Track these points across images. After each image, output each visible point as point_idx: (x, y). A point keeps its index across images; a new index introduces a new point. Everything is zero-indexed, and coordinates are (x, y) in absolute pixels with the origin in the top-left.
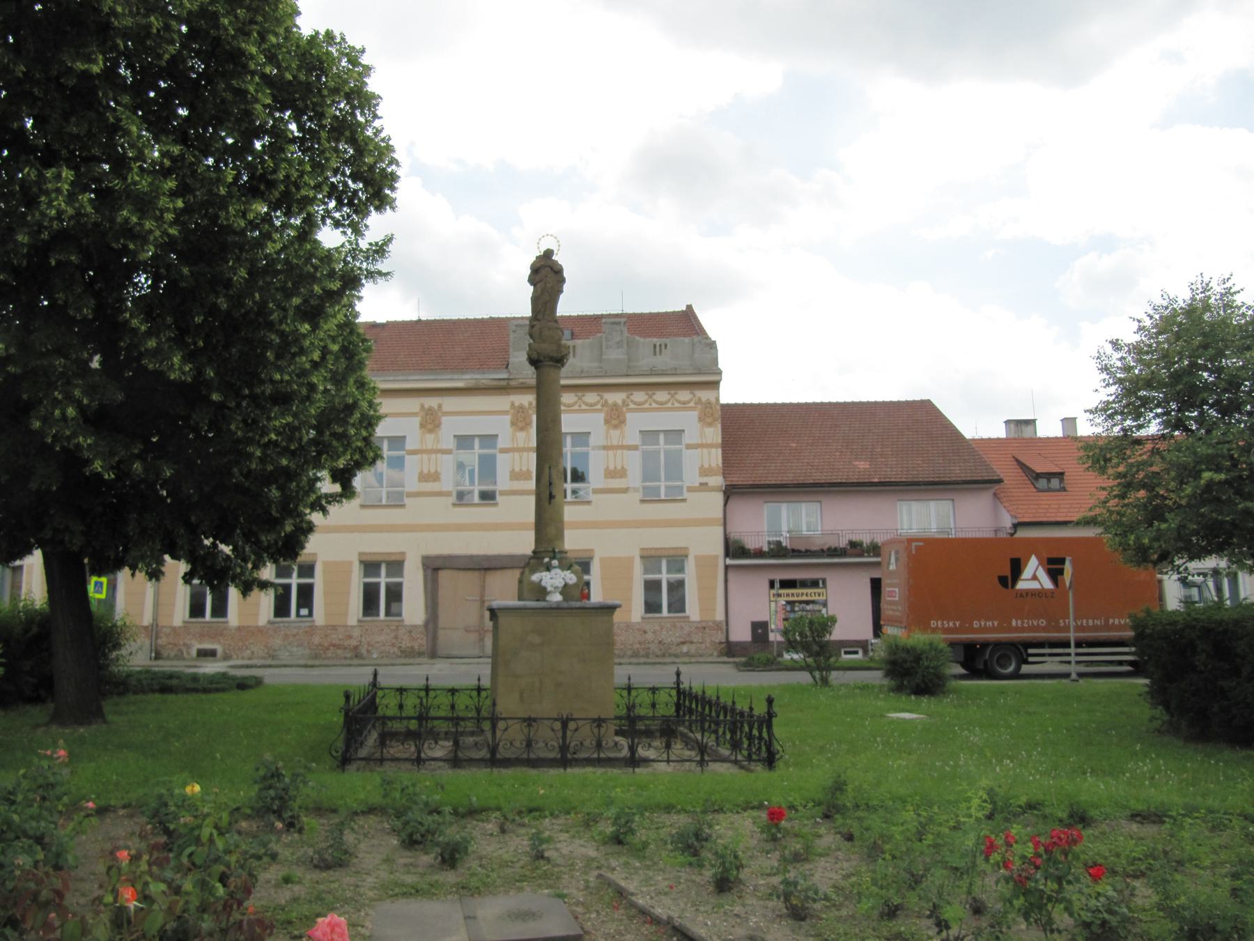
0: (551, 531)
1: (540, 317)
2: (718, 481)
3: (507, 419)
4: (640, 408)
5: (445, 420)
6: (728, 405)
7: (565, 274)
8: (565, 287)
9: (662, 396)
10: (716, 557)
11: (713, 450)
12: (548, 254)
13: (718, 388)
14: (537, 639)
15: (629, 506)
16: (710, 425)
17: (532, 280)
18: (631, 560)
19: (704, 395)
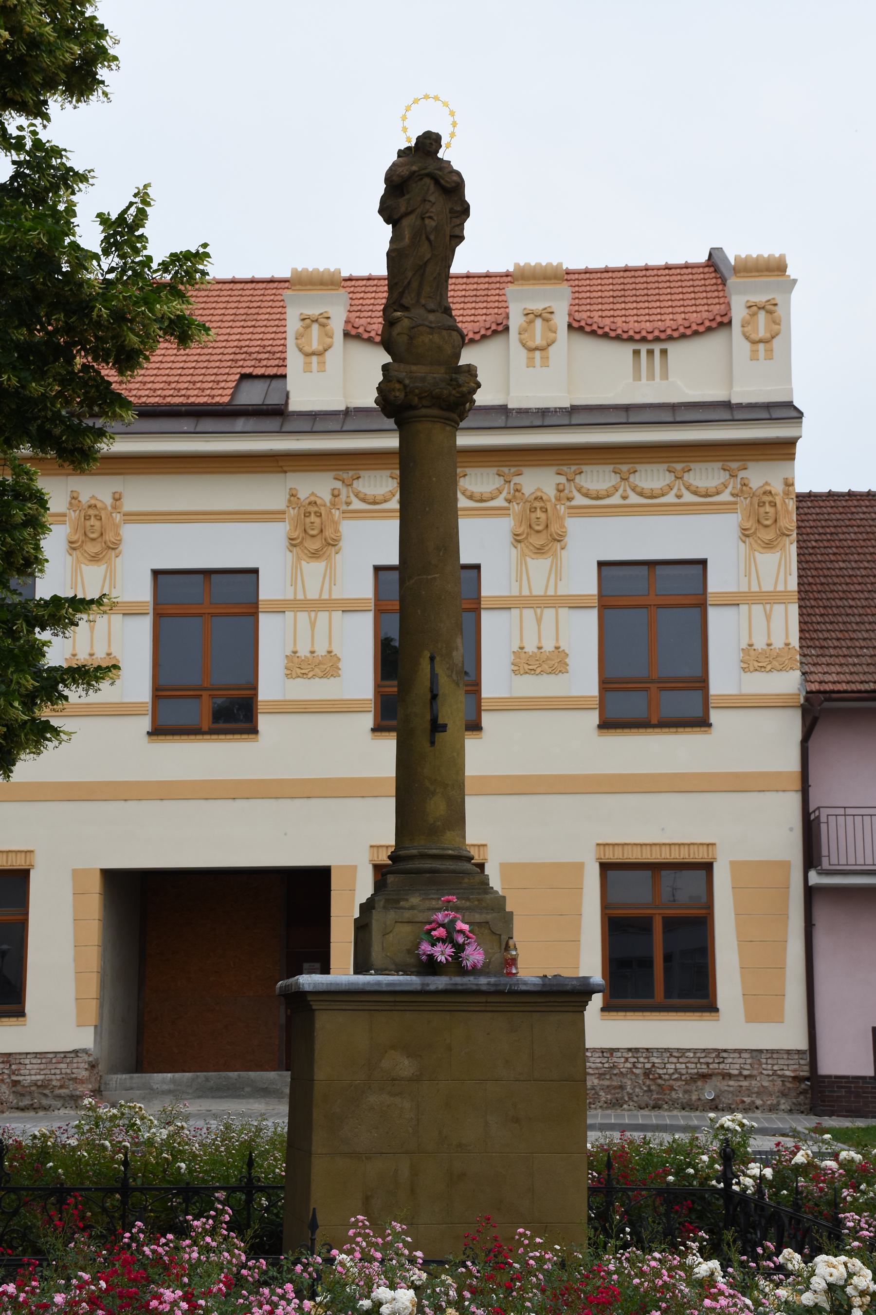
0: (437, 807)
1: (407, 300)
2: (789, 682)
3: (279, 531)
4: (598, 506)
5: (130, 533)
6: (810, 496)
7: (470, 195)
8: (469, 227)
9: (652, 477)
10: (785, 865)
11: (778, 610)
12: (428, 143)
13: (791, 457)
14: (405, 1066)
15: (577, 742)
16: (769, 546)
17: (387, 211)
18: (579, 867)
19: (760, 476)
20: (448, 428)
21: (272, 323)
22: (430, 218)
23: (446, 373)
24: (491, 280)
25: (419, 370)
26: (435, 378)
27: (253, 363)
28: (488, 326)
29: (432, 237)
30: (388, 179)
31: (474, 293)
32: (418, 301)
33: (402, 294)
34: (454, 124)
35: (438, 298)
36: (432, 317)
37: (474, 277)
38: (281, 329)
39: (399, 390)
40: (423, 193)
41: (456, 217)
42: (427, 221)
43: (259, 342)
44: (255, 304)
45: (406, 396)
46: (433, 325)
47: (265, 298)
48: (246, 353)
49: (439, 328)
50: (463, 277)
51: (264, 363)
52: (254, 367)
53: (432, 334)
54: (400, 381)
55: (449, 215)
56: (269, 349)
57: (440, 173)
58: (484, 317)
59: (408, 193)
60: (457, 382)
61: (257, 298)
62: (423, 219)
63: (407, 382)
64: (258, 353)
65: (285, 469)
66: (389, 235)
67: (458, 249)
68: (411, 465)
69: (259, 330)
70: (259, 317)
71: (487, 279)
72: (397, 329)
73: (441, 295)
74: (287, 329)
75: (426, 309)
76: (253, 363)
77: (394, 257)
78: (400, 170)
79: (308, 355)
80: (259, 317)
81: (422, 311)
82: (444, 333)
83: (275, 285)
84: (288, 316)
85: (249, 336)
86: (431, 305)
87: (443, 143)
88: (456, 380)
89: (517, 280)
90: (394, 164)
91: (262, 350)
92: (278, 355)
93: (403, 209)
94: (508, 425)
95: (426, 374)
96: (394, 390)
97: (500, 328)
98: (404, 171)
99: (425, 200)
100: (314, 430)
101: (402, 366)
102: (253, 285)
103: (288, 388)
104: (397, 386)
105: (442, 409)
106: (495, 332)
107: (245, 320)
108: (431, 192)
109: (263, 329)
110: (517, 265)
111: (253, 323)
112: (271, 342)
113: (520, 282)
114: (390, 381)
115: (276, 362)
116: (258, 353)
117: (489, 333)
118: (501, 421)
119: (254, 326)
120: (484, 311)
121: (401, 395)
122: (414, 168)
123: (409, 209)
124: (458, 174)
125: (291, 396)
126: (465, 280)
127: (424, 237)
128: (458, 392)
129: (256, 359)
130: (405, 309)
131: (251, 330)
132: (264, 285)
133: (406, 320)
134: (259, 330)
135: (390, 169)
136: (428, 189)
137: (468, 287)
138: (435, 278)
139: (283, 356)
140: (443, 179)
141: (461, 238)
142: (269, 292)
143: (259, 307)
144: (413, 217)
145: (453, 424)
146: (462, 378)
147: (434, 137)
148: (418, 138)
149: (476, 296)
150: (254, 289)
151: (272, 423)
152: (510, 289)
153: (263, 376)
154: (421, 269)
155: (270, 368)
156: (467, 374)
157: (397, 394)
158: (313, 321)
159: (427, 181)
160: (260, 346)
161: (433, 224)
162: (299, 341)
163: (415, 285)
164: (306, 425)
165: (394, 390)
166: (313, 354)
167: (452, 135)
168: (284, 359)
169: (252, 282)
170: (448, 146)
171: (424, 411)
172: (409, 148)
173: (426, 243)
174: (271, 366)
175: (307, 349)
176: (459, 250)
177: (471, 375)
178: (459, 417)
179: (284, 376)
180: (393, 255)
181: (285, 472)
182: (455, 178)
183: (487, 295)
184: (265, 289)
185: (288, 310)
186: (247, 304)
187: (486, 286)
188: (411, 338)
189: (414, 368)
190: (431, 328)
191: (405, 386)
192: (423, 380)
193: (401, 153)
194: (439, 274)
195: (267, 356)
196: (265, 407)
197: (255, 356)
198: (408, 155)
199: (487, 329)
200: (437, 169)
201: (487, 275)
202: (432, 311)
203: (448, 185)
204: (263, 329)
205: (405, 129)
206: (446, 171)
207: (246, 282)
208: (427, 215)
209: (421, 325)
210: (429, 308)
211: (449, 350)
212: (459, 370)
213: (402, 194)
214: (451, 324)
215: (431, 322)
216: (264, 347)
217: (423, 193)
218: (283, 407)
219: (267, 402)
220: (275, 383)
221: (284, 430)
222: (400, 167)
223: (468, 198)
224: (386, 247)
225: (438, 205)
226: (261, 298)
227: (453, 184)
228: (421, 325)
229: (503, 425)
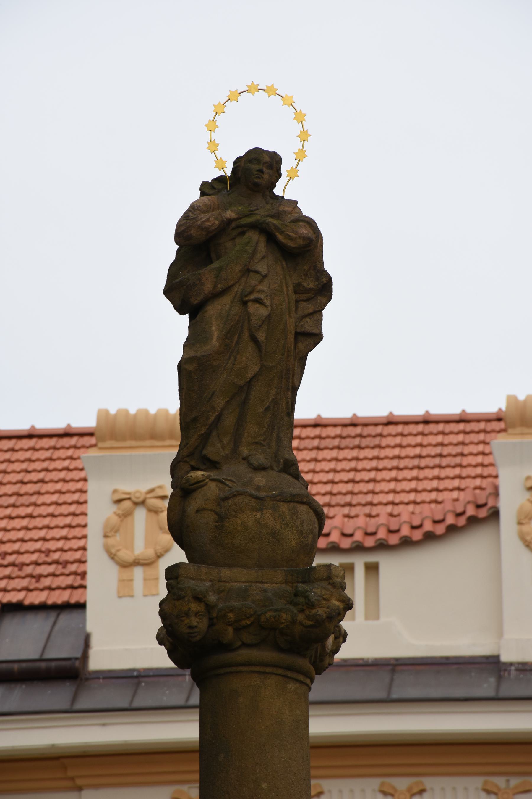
1: (215, 449)
7: (331, 261)
8: (331, 316)
12: (257, 171)
17: (180, 291)
20: (292, 686)
21: (64, 509)
22: (258, 301)
23: (286, 583)
24: (469, 427)
25: (237, 577)
26: (265, 591)
27: (25, 583)
28: (460, 510)
29: (261, 336)
30: (182, 234)
31: (438, 450)
32: (235, 451)
33: (205, 439)
34: (304, 136)
35: (274, 444)
36: (260, 479)
37: (437, 422)
38: (79, 520)
39: (197, 614)
40: (248, 262)
41: (307, 300)
42: (252, 308)
43: (38, 545)
44: (34, 477)
45: (211, 625)
46: (263, 494)
47: (52, 465)
48: (13, 564)
49: (273, 498)
50: (417, 423)
51: (47, 582)
52: (28, 589)
53: (260, 510)
54: (198, 599)
55: (294, 297)
56: (56, 556)
57: (276, 222)
58: (455, 494)
59: (218, 257)
60: (307, 597)
61: (38, 466)
62: (245, 303)
63: (212, 598)
64: (37, 564)
65: (79, 782)
66: (184, 334)
67: (311, 356)
68: (221, 757)
69: (39, 522)
70: (41, 500)
71: (461, 426)
72: (197, 501)
73: (279, 439)
74: (90, 520)
75: (250, 465)
76: (25, 583)
77: (191, 373)
78: (204, 217)
79: (126, 565)
80: (41, 500)
81: (242, 469)
82: (284, 507)
83: (73, 441)
84: (90, 496)
85: (21, 534)
86: (260, 458)
87: (283, 171)
88: (305, 595)
89: (513, 425)
90: (193, 208)
91: (43, 558)
92: (73, 568)
93: (208, 287)
94: (502, 694)
95: (251, 585)
96: (187, 614)
97: (483, 513)
98: (212, 221)
99: (249, 271)
100: (136, 704)
101: (204, 569)
102: (32, 443)
103: (90, 627)
104: (194, 606)
105: (280, 649)
106: (473, 521)
107: (14, 506)
108: (259, 256)
109: (47, 521)
110: (512, 400)
111: (29, 510)
112: (60, 544)
113: (519, 430)
114: (180, 598)
115: (69, 581)
116: (37, 564)
117: (462, 521)
118: (487, 688)
119: (31, 516)
120: (456, 483)
121: (201, 624)
122: (230, 214)
123: (220, 287)
124: (311, 223)
125: (94, 642)
126: (420, 428)
127: (246, 335)
128: (308, 617)
129: (31, 576)
130: (212, 464)
131: (25, 522)
132: (52, 442)
133: (213, 485)
134: (39, 522)
135: (186, 217)
136: (254, 252)
137: (426, 440)
138: (267, 409)
139: (81, 568)
140: (282, 232)
141: (317, 337)
142: (62, 453)
143: (42, 481)
144: (227, 300)
145: (301, 678)
146: (316, 591)
147: (267, 158)
148: (238, 161)
149: (441, 455)
150: (34, 449)
151: (57, 695)
152: (499, 443)
153: (43, 607)
154: (242, 391)
155: (57, 592)
156: (324, 584)
157: (194, 621)
158: (136, 504)
159: (253, 236)
160: (40, 551)
161: (264, 312)
162: (110, 541)
163: (229, 421)
164: (118, 697)
165: (187, 614)
166: (136, 563)
167: (300, 155)
168: (83, 575)
169: (30, 436)
170: (293, 174)
171: (245, 654)
172: (220, 180)
173: (251, 346)
174: (59, 588)
175: (125, 555)
176: (315, 358)
177: (334, 585)
178: (314, 664)
179: (81, 606)
180: (190, 367)
181: (80, 789)
182: (304, 231)
183: (462, 455)
184: (55, 448)
185: (91, 486)
186: (19, 477)
187: (461, 438)
188: (221, 518)
189: (226, 573)
190: (257, 498)
191: (209, 607)
192: (244, 594)
193: (206, 188)
194: (275, 402)
195: (51, 569)
196: (43, 665)
197: (29, 570)
198: (219, 191)
199: (459, 515)
200: (272, 216)
201: (463, 419)
202: (260, 468)
203: (291, 244)
204: (47, 521)
205: (213, 146)
206: (289, 218)
207: (19, 437)
208: (252, 297)
209: (240, 494)
210: (255, 463)
211: (291, 539)
212: (309, 575)
213: (209, 261)
214: (296, 491)
215: (258, 488)
216: (48, 552)
217: (248, 262)
218: (77, 663)
219: (50, 654)
220: (66, 619)
221: (77, 706)
222: (203, 212)
223: (328, 266)
224: (178, 354)
225: (272, 279)
226: (45, 465)
227: (301, 242)
228: (240, 494)
229: (491, 693)
